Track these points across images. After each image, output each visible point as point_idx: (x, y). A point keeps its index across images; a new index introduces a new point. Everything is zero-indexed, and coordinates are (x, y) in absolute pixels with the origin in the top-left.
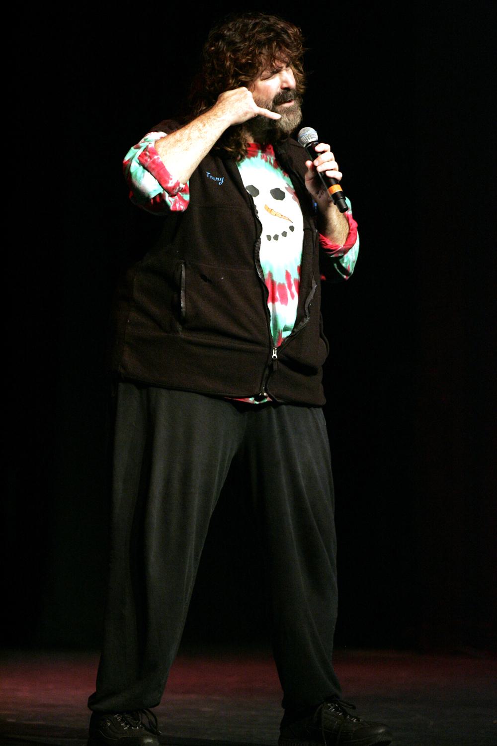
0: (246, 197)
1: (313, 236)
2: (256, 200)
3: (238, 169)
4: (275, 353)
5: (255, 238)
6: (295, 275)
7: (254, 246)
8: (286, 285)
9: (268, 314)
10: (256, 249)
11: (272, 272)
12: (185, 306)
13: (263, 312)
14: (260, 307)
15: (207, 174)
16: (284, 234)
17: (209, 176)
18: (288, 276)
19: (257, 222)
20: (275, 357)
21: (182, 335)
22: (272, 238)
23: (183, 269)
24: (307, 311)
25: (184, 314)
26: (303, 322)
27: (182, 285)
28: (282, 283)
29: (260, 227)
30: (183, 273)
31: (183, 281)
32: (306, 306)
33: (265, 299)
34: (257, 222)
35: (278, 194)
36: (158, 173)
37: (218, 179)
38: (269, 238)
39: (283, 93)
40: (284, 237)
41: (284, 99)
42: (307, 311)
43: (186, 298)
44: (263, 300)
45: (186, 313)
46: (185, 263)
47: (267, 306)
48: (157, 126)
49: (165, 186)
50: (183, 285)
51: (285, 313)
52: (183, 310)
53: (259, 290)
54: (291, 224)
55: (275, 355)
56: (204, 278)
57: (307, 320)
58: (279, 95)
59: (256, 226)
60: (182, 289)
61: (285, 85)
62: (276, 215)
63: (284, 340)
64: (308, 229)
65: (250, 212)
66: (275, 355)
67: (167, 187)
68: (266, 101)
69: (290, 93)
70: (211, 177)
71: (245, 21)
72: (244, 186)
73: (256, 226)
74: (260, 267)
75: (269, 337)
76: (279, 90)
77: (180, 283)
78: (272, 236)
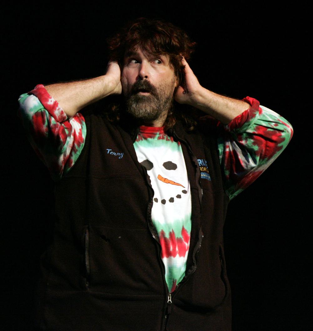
1: (200, 201)
2: (149, 173)
4: (170, 299)
6: (189, 228)
7: (147, 207)
8: (183, 239)
9: (159, 249)
10: (149, 211)
16: (164, 202)
18: (184, 231)
19: (150, 190)
20: (170, 302)
24: (194, 259)
25: (88, 271)
26: (191, 269)
28: (179, 237)
32: (194, 255)
34: (150, 190)
35: (170, 166)
36: (40, 94)
38: (164, 202)
42: (194, 259)
43: (89, 257)
45: (90, 270)
46: (89, 228)
49: (45, 103)
50: (87, 246)
51: (177, 265)
52: (88, 267)
54: (184, 189)
55: (169, 300)
57: (195, 268)
62: (169, 183)
63: (163, 257)
66: (169, 300)
67: (47, 105)
72: (175, 237)
75: (164, 285)
77: (85, 241)
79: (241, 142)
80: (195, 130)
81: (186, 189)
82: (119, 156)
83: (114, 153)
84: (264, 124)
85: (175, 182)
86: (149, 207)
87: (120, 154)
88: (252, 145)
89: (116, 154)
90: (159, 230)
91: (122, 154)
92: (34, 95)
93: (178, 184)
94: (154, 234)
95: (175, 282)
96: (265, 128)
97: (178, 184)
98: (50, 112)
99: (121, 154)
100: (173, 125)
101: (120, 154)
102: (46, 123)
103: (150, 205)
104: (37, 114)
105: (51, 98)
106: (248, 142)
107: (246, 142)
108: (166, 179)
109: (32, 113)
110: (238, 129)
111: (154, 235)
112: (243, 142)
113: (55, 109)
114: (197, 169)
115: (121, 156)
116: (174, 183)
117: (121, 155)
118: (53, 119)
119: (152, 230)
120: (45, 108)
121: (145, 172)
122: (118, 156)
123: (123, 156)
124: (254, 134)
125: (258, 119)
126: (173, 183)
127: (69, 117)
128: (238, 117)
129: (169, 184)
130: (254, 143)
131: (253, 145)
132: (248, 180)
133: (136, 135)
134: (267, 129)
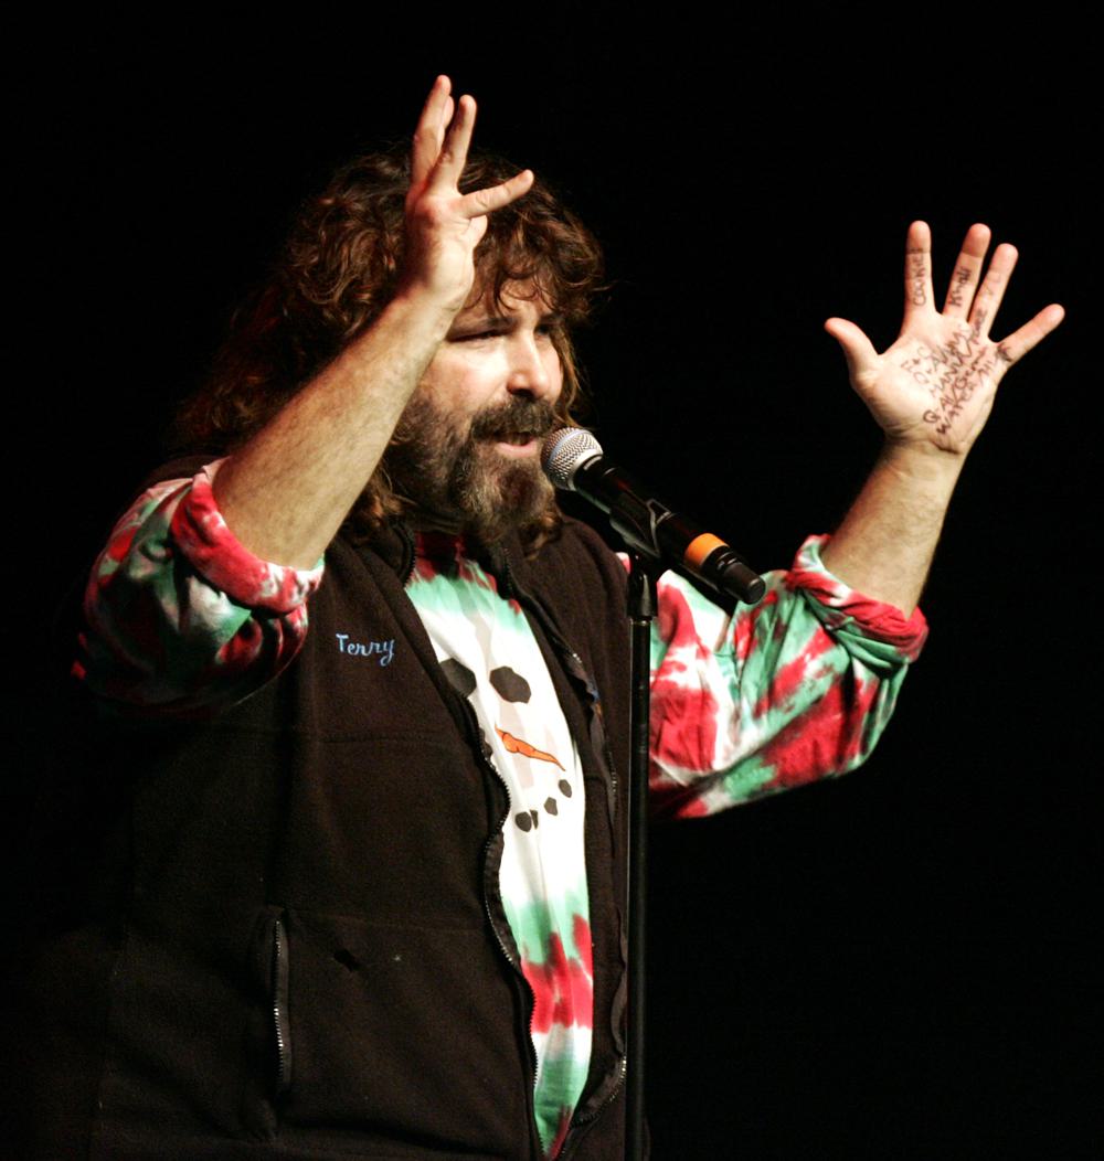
0: (448, 690)
3: (405, 595)
5: (485, 833)
7: (482, 857)
9: (529, 1058)
10: (489, 863)
12: (289, 1051)
13: (513, 1055)
14: (511, 1041)
16: (551, 806)
17: (346, 648)
21: (279, 1143)
23: (281, 934)
25: (287, 1078)
27: (280, 985)
29: (503, 799)
30: (281, 945)
31: (283, 969)
32: (615, 1023)
33: (523, 1016)
34: (491, 781)
37: (378, 645)
39: (515, 405)
40: (551, 815)
41: (513, 425)
44: (517, 1016)
45: (293, 1072)
46: (285, 918)
47: (530, 1040)
48: (736, 802)
50: (282, 984)
51: (567, 1049)
52: (286, 1063)
53: (502, 988)
56: (346, 958)
58: (501, 410)
59: (488, 799)
60: (279, 995)
61: (521, 382)
62: (518, 751)
64: (592, 778)
65: (459, 749)
68: (451, 413)
69: (534, 408)
73: (488, 799)
74: (502, 917)
75: (531, 1136)
76: (500, 396)
77: (274, 982)
82: (381, 655)
83: (372, 644)
85: (535, 750)
86: (492, 850)
87: (381, 648)
89: (367, 650)
91: (388, 646)
95: (565, 1114)
97: (546, 757)
99: (385, 644)
100: (899, 654)
103: (496, 842)
108: (505, 733)
113: (291, 595)
114: (593, 707)
115: (386, 653)
116: (558, 764)
117: (387, 651)
119: (502, 933)
122: (376, 657)
123: (394, 651)
132: (376, 595)
133: (408, 564)
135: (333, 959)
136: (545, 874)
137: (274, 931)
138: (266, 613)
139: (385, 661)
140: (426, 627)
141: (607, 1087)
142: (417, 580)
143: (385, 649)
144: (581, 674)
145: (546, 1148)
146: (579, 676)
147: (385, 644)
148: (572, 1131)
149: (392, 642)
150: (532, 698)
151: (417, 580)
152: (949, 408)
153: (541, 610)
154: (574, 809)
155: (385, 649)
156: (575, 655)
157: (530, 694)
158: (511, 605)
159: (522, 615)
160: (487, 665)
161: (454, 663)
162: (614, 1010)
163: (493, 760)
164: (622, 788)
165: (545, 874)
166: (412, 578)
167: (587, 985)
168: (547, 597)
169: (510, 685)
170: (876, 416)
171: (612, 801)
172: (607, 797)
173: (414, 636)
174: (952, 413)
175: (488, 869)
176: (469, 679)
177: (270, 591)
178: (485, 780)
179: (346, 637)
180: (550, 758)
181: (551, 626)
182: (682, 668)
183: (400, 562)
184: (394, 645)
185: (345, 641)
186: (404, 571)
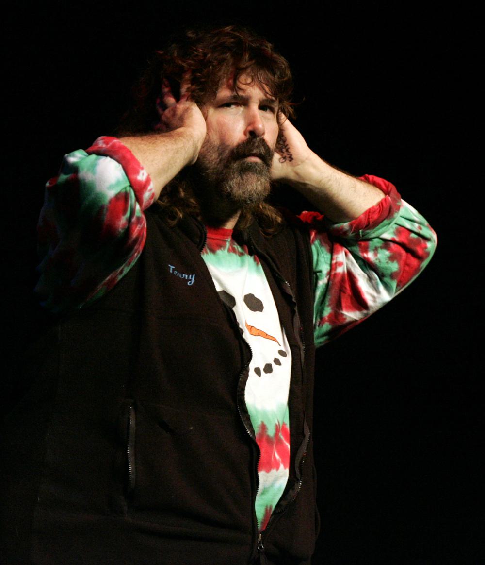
0: (224, 304)
9: (255, 454)
11: (266, 423)
15: (170, 267)
22: (262, 372)
24: (297, 470)
26: (293, 489)
30: (132, 422)
31: (132, 431)
32: (297, 465)
36: (124, 158)
38: (257, 371)
42: (297, 470)
49: (133, 177)
51: (273, 483)
52: (132, 476)
61: (282, 160)
62: (259, 335)
65: (226, 327)
67: (136, 179)
70: (175, 272)
71: (258, 45)
77: (128, 429)
78: (262, 368)
79: (365, 255)
80: (289, 229)
81: (282, 348)
84: (408, 225)
85: (267, 335)
86: (242, 378)
87: (188, 277)
88: (387, 261)
90: (256, 423)
91: (192, 277)
92: (111, 157)
93: (273, 339)
94: (248, 426)
96: (408, 232)
97: (270, 338)
98: (137, 194)
99: (190, 276)
101: (188, 277)
102: (128, 214)
104: (118, 197)
105: (142, 168)
106: (379, 256)
107: (376, 254)
108: (252, 327)
109: (111, 194)
110: (368, 231)
111: (249, 429)
112: (370, 255)
115: (191, 280)
116: (266, 336)
118: (138, 207)
120: (131, 186)
121: (232, 317)
123: (195, 279)
124: (393, 241)
125: (401, 217)
126: (265, 336)
127: (378, 247)
128: (373, 208)
129: (259, 337)
130: (392, 258)
131: (390, 262)
134: (409, 234)
135: (158, 426)
136: (268, 396)
137: (129, 411)
138: (139, 189)
139: (190, 283)
140: (211, 274)
141: (290, 495)
142: (207, 253)
143: (190, 278)
144: (290, 292)
145: (259, 526)
146: (289, 293)
147: (190, 276)
148: (273, 517)
149: (194, 275)
150: (264, 310)
151: (207, 253)
152: (284, 150)
153: (270, 259)
154: (287, 362)
155: (190, 278)
156: (286, 282)
157: (262, 303)
158: (255, 260)
159: (260, 266)
160: (243, 293)
161: (225, 293)
162: (297, 458)
163: (244, 336)
164: (306, 358)
165: (268, 396)
166: (204, 251)
167: (288, 448)
168: (273, 254)
169: (254, 304)
170: (348, 172)
171: (303, 361)
172: (300, 354)
173: (205, 277)
174: (287, 150)
175: (239, 387)
176: (232, 300)
177: (142, 177)
178: (240, 344)
179: (174, 267)
180: (274, 339)
181: (275, 267)
182: (341, 264)
183: (198, 241)
184: (195, 277)
185: (173, 268)
186: (200, 246)
